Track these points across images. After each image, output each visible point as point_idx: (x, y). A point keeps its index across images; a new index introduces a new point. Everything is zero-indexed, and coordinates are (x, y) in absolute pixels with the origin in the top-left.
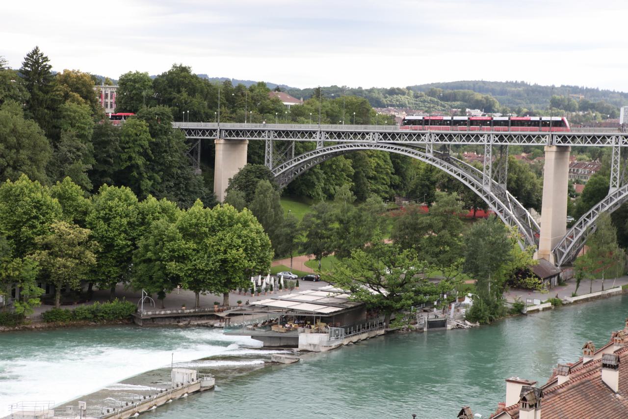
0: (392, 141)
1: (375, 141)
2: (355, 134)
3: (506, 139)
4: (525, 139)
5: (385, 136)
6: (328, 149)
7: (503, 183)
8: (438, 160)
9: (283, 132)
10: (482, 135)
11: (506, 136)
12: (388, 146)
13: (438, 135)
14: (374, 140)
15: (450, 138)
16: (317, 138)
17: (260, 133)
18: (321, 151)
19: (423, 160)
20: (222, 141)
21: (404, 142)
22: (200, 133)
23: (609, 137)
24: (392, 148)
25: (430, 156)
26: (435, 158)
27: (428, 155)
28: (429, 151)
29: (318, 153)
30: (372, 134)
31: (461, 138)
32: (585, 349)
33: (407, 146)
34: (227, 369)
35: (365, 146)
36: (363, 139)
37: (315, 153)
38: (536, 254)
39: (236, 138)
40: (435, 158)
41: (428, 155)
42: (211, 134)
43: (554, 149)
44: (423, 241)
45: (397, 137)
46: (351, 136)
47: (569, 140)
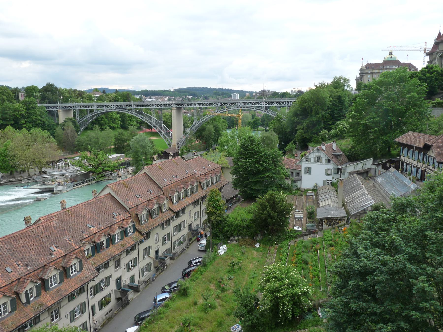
5: (118, 106)
15: (203, 104)
17: (92, 106)
20: (61, 110)
25: (134, 112)
27: (133, 112)
38: (171, 146)
43: (175, 109)
47: (274, 103)
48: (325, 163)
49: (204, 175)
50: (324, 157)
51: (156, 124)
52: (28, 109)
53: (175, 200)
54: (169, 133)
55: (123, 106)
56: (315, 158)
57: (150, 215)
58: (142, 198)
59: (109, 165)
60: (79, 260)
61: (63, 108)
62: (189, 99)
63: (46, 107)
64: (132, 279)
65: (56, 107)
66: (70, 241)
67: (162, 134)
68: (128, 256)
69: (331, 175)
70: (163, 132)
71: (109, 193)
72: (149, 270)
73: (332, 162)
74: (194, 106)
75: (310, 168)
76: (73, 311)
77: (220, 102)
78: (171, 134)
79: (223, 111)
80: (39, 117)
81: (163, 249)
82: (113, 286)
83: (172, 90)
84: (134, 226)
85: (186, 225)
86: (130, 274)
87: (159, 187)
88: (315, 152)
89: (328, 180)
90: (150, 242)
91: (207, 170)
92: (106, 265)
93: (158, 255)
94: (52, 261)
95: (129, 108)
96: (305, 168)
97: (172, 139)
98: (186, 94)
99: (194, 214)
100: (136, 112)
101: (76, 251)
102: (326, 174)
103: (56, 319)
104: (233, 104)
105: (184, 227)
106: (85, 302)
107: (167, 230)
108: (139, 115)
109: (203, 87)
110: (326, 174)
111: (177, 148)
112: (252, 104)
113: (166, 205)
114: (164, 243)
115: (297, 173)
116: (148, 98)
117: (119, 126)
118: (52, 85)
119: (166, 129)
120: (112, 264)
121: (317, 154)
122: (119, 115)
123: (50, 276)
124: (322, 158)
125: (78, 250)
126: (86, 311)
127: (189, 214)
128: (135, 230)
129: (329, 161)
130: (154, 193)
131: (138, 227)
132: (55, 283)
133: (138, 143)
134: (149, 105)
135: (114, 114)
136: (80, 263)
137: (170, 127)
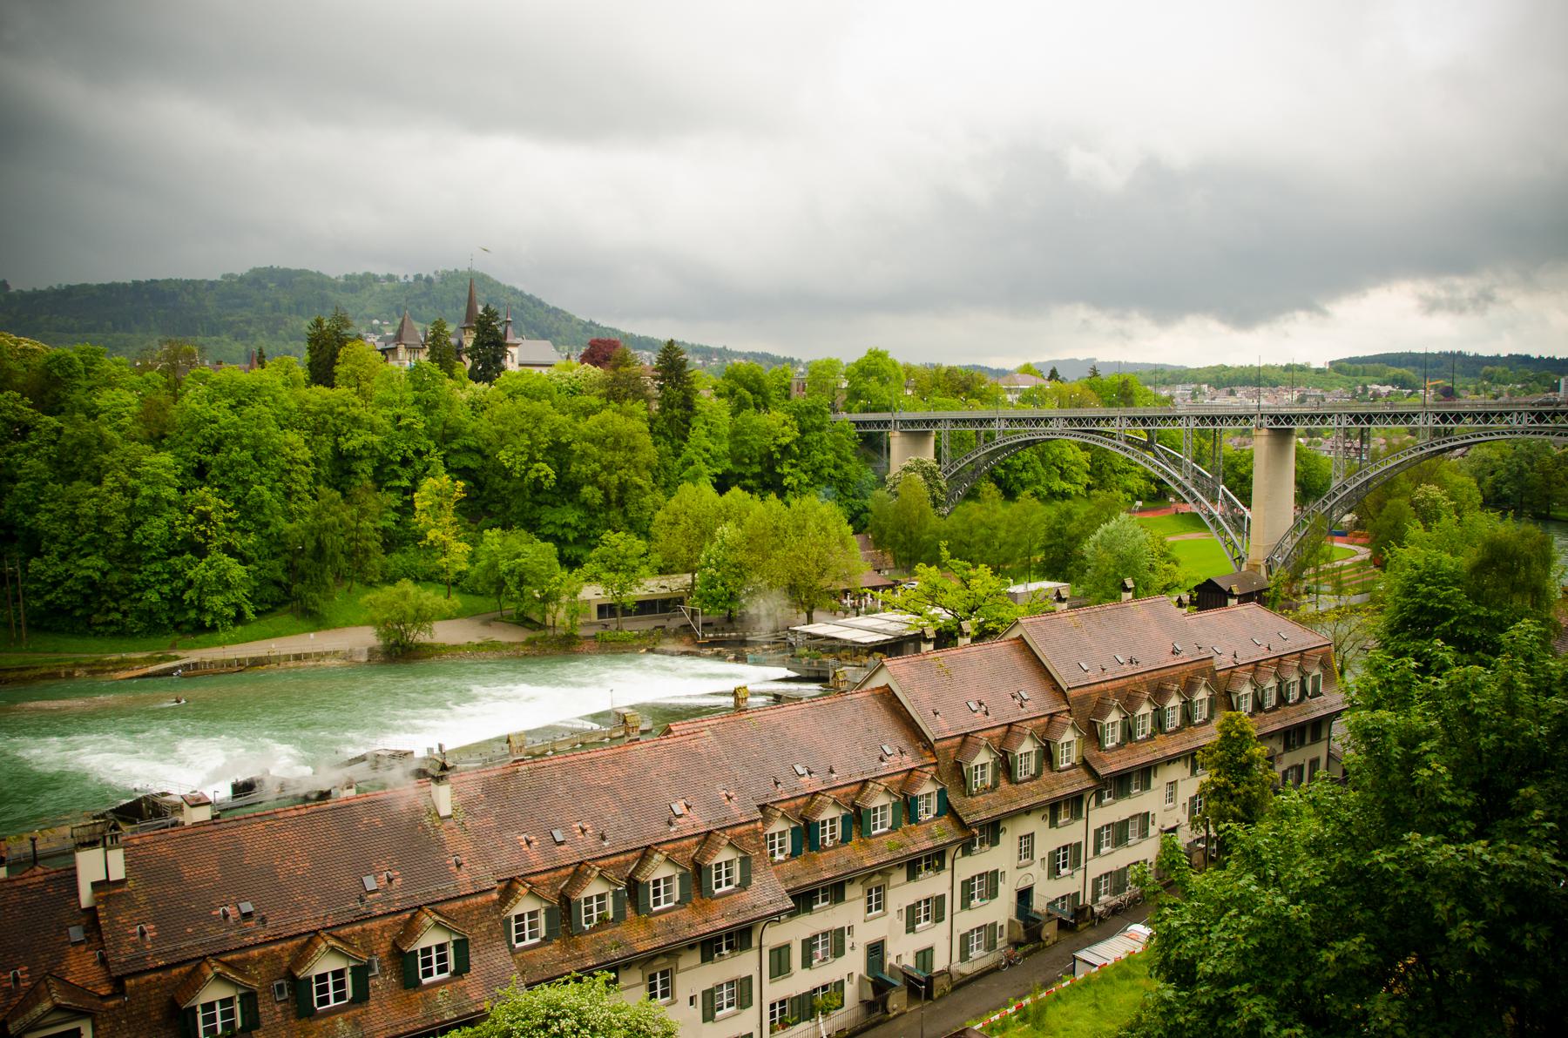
5: (1070, 420)
10: (1415, 415)
11: (1451, 414)
13: (1438, 415)
16: (995, 427)
23: (1415, 415)
27: (1117, 442)
31: (1475, 419)
34: (270, 611)
41: (1117, 442)
42: (886, 426)
43: (1265, 432)
46: (1306, 420)
47: (1548, 418)
49: (1250, 667)
51: (1196, 484)
52: (803, 431)
53: (1112, 738)
54: (1242, 518)
57: (1006, 767)
58: (987, 714)
59: (1000, 615)
60: (740, 855)
61: (906, 426)
62: (1376, 395)
63: (858, 424)
64: (925, 956)
65: (886, 423)
66: (729, 798)
68: (912, 884)
71: (887, 686)
72: (991, 946)
74: (1184, 426)
76: (711, 991)
80: (830, 456)
81: (1047, 892)
82: (853, 964)
83: (1314, 366)
84: (942, 793)
85: (1153, 830)
86: (920, 941)
87: (1056, 687)
90: (999, 857)
92: (836, 891)
93: (1028, 905)
94: (668, 841)
95: (1107, 429)
98: (1365, 379)
99: (1192, 799)
101: (742, 829)
103: (662, 997)
105: (1144, 833)
106: (750, 978)
107: (1072, 832)
109: (1446, 354)
111: (1263, 573)
112: (1385, 420)
113: (1074, 748)
114: (1054, 872)
116: (1223, 391)
117: (1081, 489)
119: (1233, 502)
120: (855, 893)
122: (1089, 455)
123: (655, 877)
125: (747, 827)
126: (750, 1004)
128: (946, 808)
130: (1037, 703)
131: (955, 799)
132: (667, 900)
133: (1109, 548)
135: (1068, 450)
136: (745, 861)
137: (1246, 498)
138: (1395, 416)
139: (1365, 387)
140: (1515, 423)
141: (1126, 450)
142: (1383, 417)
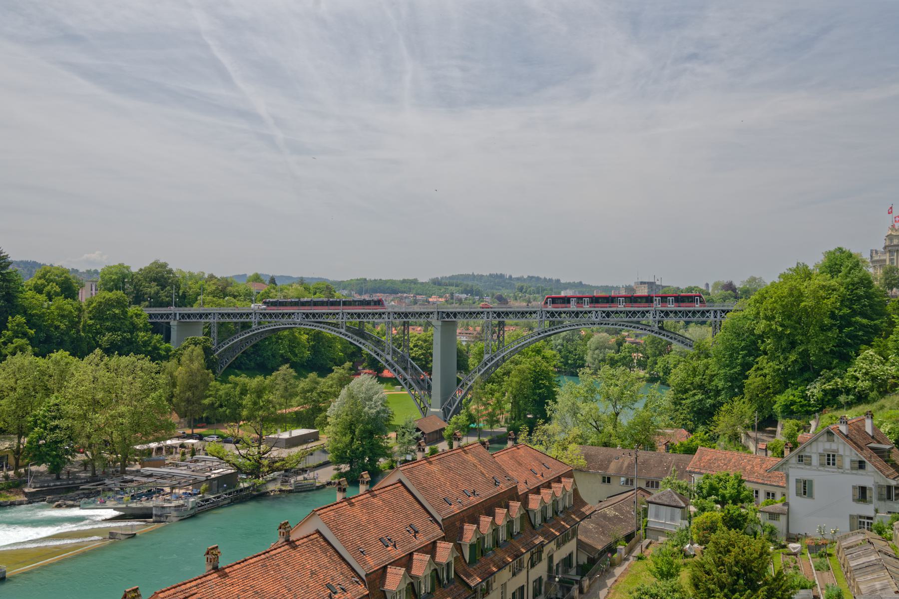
0: (313, 320)
1: (299, 320)
2: (283, 315)
3: (503, 315)
4: (573, 315)
5: (307, 315)
6: (261, 328)
7: (388, 354)
8: (350, 334)
9: (226, 314)
10: (535, 312)
12: (309, 324)
14: (597, 318)
18: (256, 329)
19: (338, 335)
21: (322, 320)
22: (165, 317)
24: (313, 325)
25: (343, 331)
26: (347, 333)
28: (342, 328)
29: (254, 331)
30: (296, 314)
31: (465, 315)
32: (208, 556)
33: (324, 323)
35: (291, 324)
36: (577, 317)
37: (251, 331)
39: (188, 320)
40: (347, 333)
44: (804, 424)
45: (362, 316)
48: (852, 468)
50: (848, 453)
55: (321, 315)
56: (821, 455)
65: (168, 316)
67: (406, 383)
69: (871, 502)
70: (408, 377)
73: (869, 466)
75: (811, 482)
77: (220, 312)
78: (428, 383)
79: (556, 331)
88: (820, 439)
89: (861, 517)
91: (541, 478)
96: (798, 481)
97: (430, 396)
100: (348, 329)
102: (854, 500)
104: (244, 317)
108: (356, 337)
110: (854, 500)
115: (768, 494)
118: (164, 266)
121: (827, 446)
124: (841, 456)
127: (502, 593)
129: (861, 465)
134: (248, 315)
138: (471, 313)
139: (452, 294)
140: (594, 319)
141: (346, 335)
142: (464, 314)
